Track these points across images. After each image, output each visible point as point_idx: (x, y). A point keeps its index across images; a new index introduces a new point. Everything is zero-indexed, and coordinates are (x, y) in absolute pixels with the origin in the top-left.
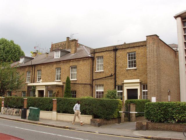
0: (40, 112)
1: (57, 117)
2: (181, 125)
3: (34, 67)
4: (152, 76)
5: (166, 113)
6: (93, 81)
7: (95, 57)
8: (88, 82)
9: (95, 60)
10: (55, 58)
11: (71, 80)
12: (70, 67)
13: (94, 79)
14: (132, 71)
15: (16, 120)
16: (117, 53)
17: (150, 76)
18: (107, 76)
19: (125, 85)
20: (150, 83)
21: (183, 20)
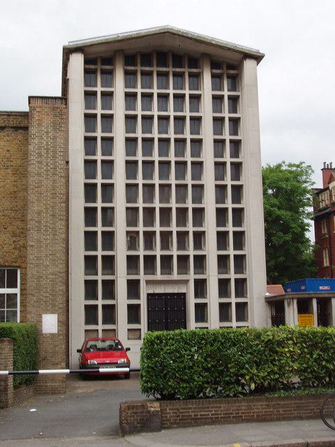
2: (268, 399)
4: (46, 240)
5: (221, 365)
17: (39, 241)
20: (38, 266)
21: (88, 66)
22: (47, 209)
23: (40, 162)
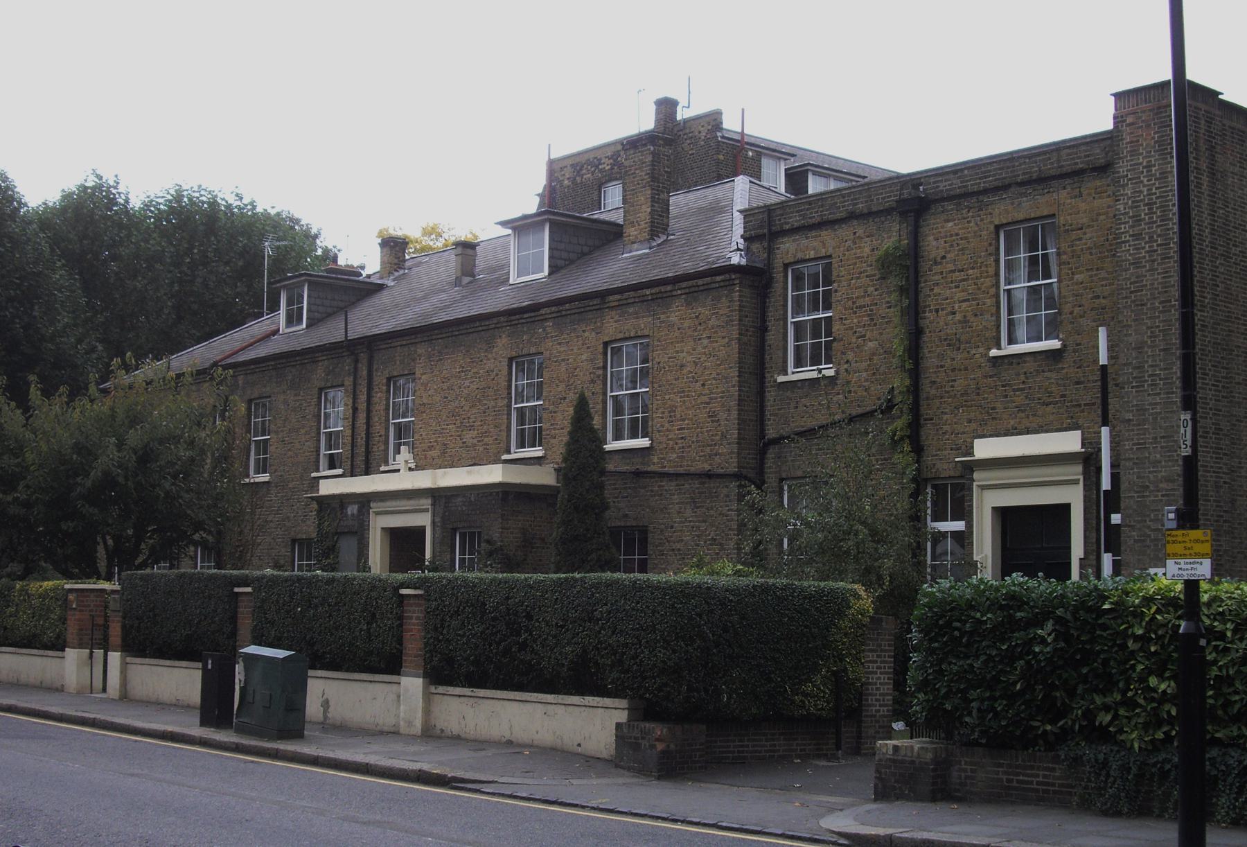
0: (310, 682)
1: (427, 711)
3: (363, 357)
6: (762, 453)
7: (778, 263)
8: (727, 458)
9: (778, 287)
10: (511, 282)
11: (612, 445)
12: (600, 348)
13: (771, 433)
14: (1030, 366)
15: (423, 778)
16: (925, 230)
18: (860, 411)
19: (980, 477)
22: (1153, 336)
23: (1138, 236)
